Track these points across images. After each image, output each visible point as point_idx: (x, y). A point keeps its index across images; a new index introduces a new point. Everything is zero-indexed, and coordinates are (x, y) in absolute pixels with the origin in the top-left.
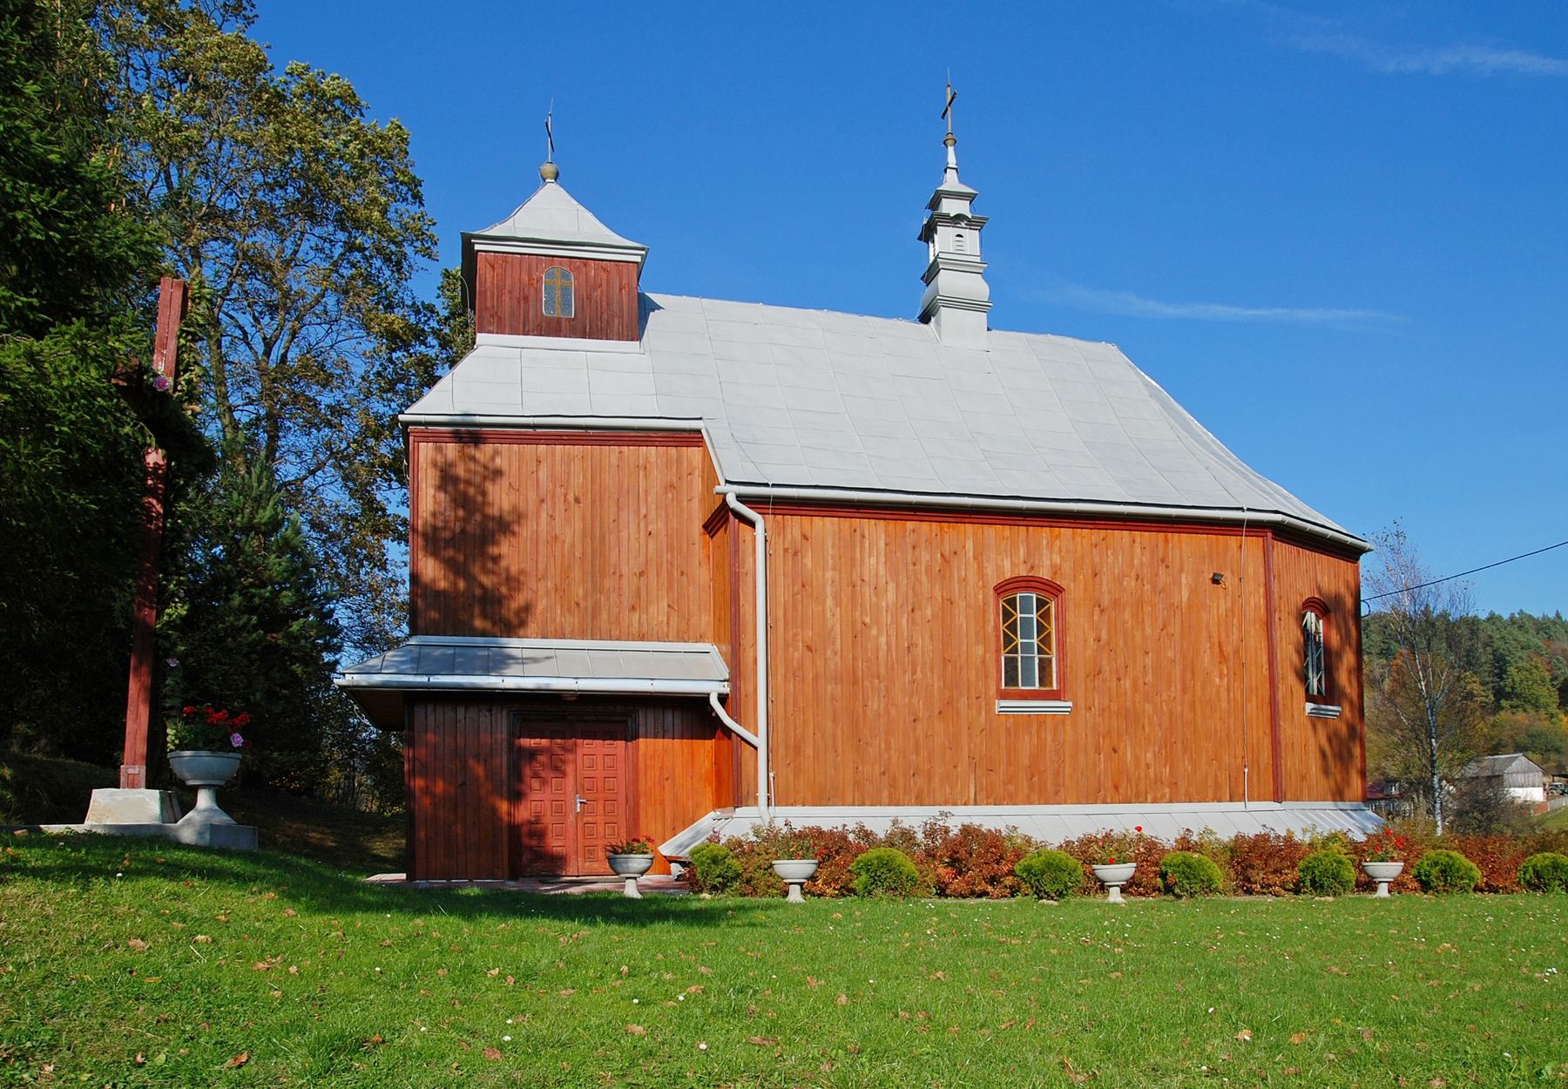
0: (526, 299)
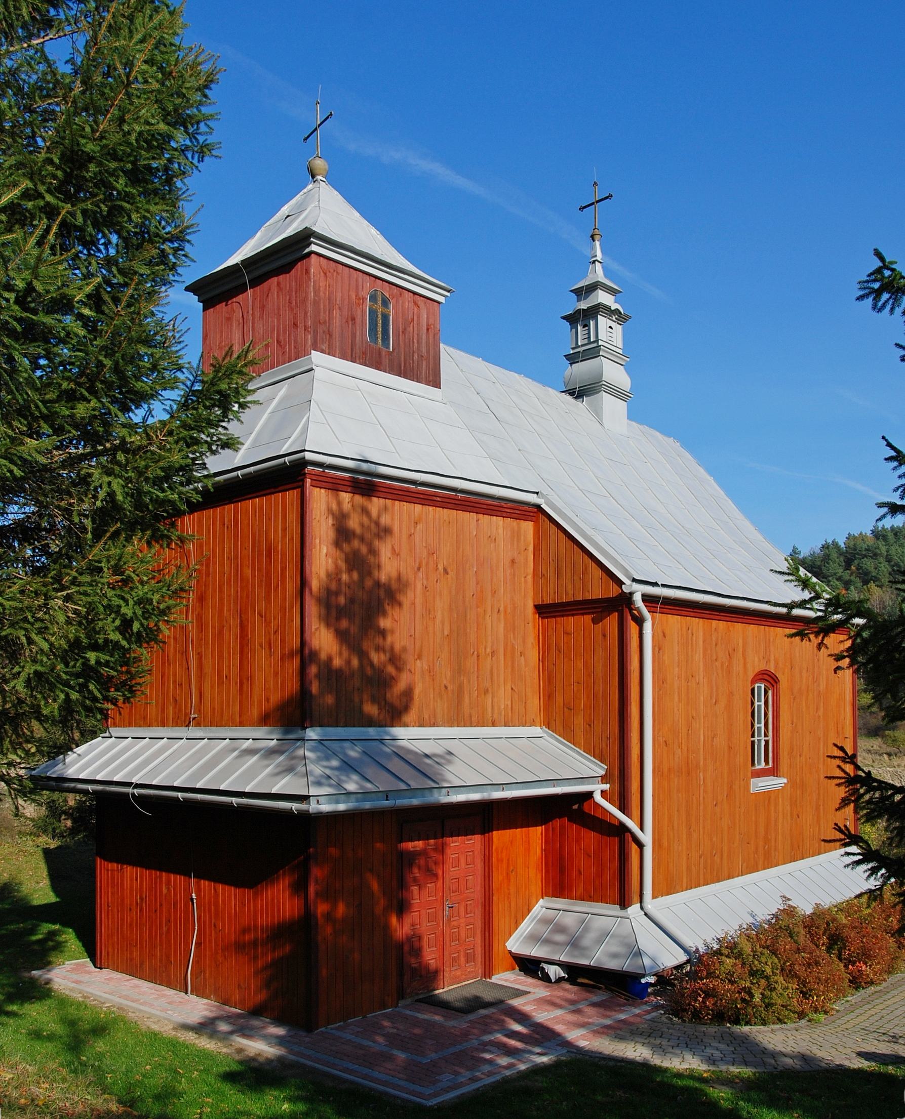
0: (353, 319)
